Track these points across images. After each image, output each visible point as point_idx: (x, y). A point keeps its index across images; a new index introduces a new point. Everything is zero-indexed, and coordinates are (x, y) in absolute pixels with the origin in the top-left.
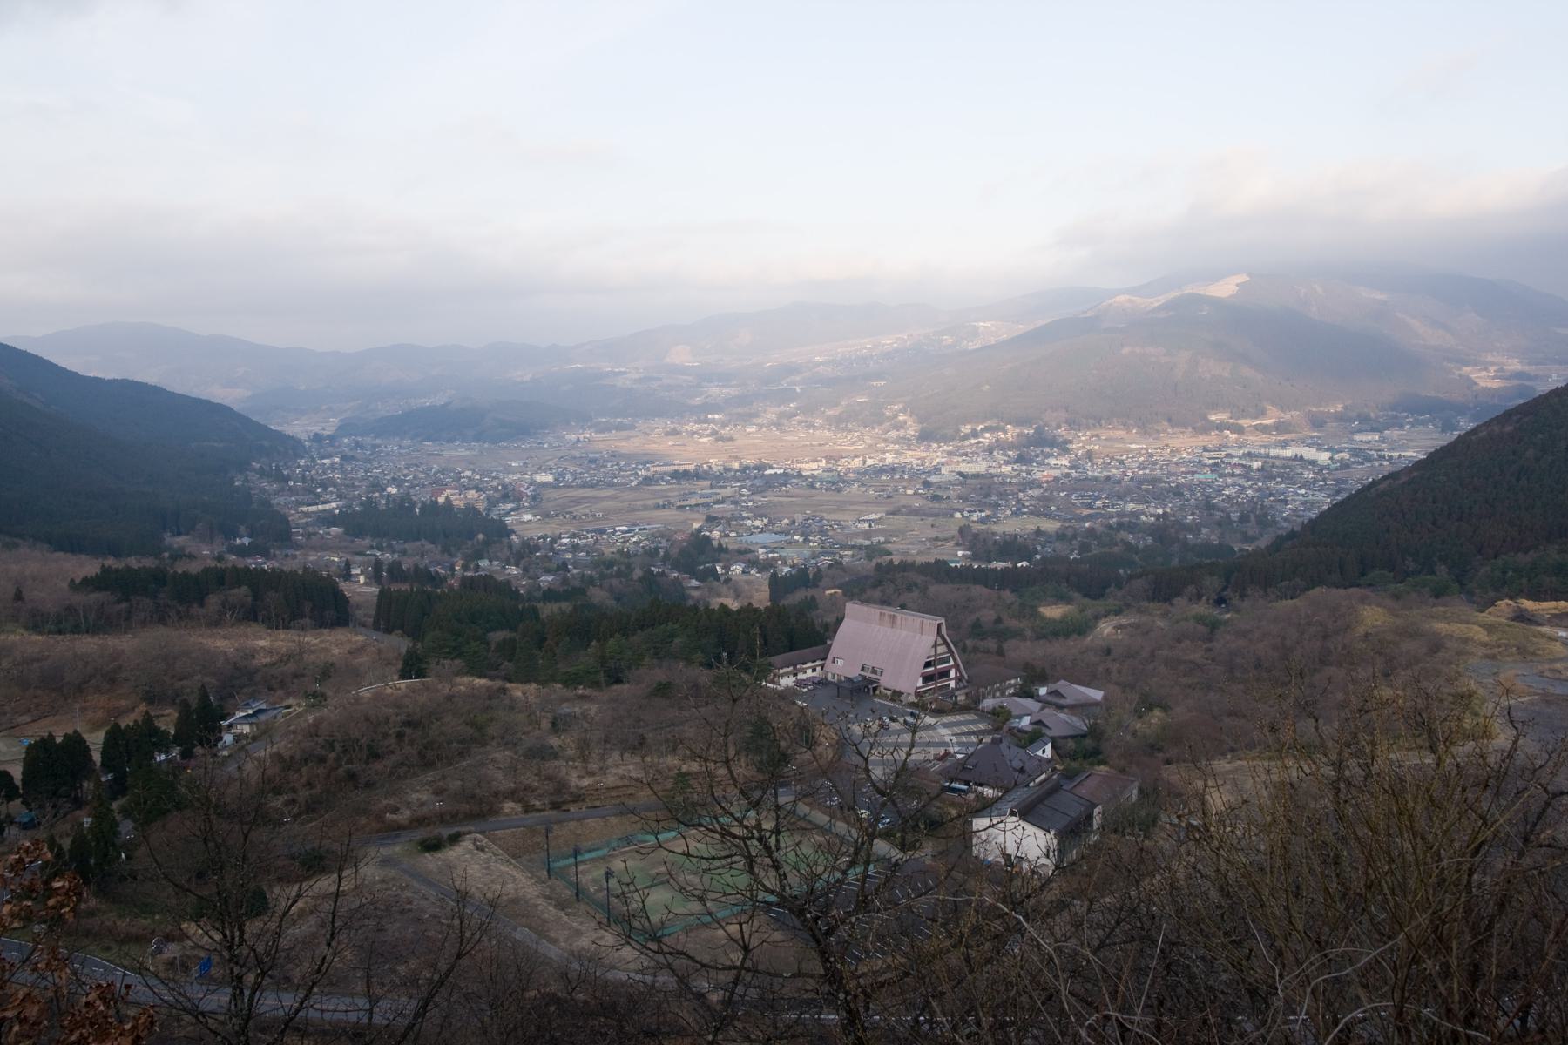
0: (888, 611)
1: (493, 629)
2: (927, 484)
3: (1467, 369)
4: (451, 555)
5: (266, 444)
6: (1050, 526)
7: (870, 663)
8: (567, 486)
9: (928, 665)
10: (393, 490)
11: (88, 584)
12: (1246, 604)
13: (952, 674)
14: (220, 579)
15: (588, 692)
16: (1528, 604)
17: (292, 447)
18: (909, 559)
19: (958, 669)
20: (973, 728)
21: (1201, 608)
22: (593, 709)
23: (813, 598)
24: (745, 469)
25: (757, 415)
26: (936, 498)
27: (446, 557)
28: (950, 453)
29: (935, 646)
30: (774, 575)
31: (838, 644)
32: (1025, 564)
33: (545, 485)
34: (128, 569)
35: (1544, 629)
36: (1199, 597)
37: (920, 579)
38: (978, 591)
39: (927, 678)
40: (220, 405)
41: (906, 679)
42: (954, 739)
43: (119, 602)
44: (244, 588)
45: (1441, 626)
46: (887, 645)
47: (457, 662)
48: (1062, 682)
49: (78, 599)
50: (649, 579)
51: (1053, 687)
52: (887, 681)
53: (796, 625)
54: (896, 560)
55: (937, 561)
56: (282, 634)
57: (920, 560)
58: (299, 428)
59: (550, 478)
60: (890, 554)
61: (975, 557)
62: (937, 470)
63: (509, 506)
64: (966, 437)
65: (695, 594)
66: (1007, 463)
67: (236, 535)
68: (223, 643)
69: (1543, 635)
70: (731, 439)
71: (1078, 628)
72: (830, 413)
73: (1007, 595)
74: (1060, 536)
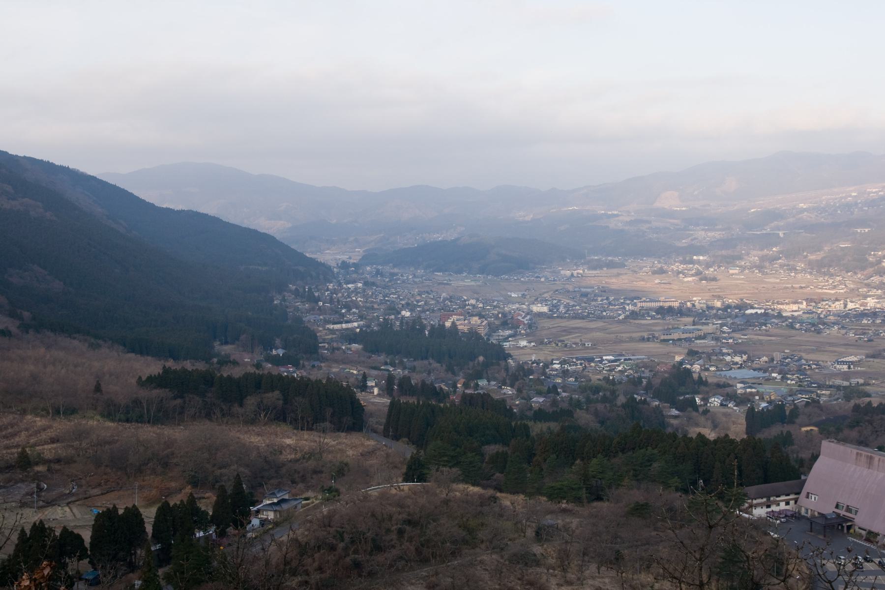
1: (488, 443)
4: (454, 373)
5: (301, 269)
8: (560, 317)
10: (406, 314)
11: (152, 381)
14: (257, 383)
15: (570, 506)
17: (322, 272)
22: (574, 522)
25: (740, 258)
27: (450, 375)
30: (751, 409)
34: (184, 371)
43: (175, 398)
44: (277, 393)
47: (454, 470)
49: (144, 394)
50: (631, 405)
52: (862, 521)
56: (306, 435)
58: (330, 256)
59: (545, 309)
60: (869, 395)
65: (675, 422)
67: (272, 346)
68: (257, 439)
70: (714, 279)
72: (812, 257)
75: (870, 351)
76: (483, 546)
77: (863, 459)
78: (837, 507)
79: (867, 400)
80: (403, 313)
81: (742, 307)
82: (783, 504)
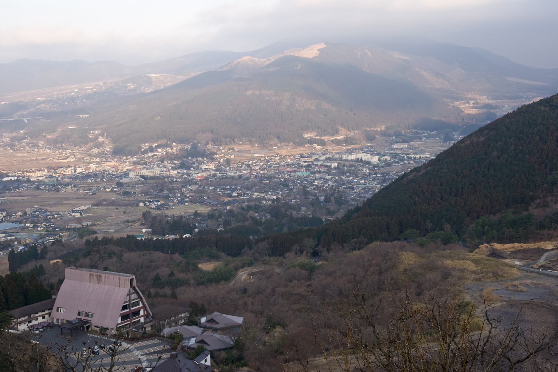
0: (95, 272)
2: (119, 184)
3: (456, 103)
6: (204, 210)
9: (124, 308)
12: (331, 254)
13: (142, 313)
16: (497, 246)
18: (109, 236)
19: (144, 307)
21: (303, 259)
23: (41, 266)
26: (126, 193)
28: (135, 163)
29: (129, 294)
30: (12, 252)
31: (60, 298)
32: (188, 235)
35: (507, 261)
36: (302, 252)
37: (117, 249)
38: (158, 255)
39: (124, 317)
45: (449, 263)
46: (96, 296)
51: (210, 317)
52: (96, 321)
54: (100, 237)
55: (129, 237)
57: (117, 236)
60: (95, 233)
61: (154, 233)
62: (126, 174)
64: (146, 152)
66: (174, 168)
69: (507, 265)
71: (224, 277)
72: (49, 137)
73: (177, 257)
74: (211, 216)
75: (94, 202)
77: (95, 277)
78: (79, 314)
79: (95, 236)
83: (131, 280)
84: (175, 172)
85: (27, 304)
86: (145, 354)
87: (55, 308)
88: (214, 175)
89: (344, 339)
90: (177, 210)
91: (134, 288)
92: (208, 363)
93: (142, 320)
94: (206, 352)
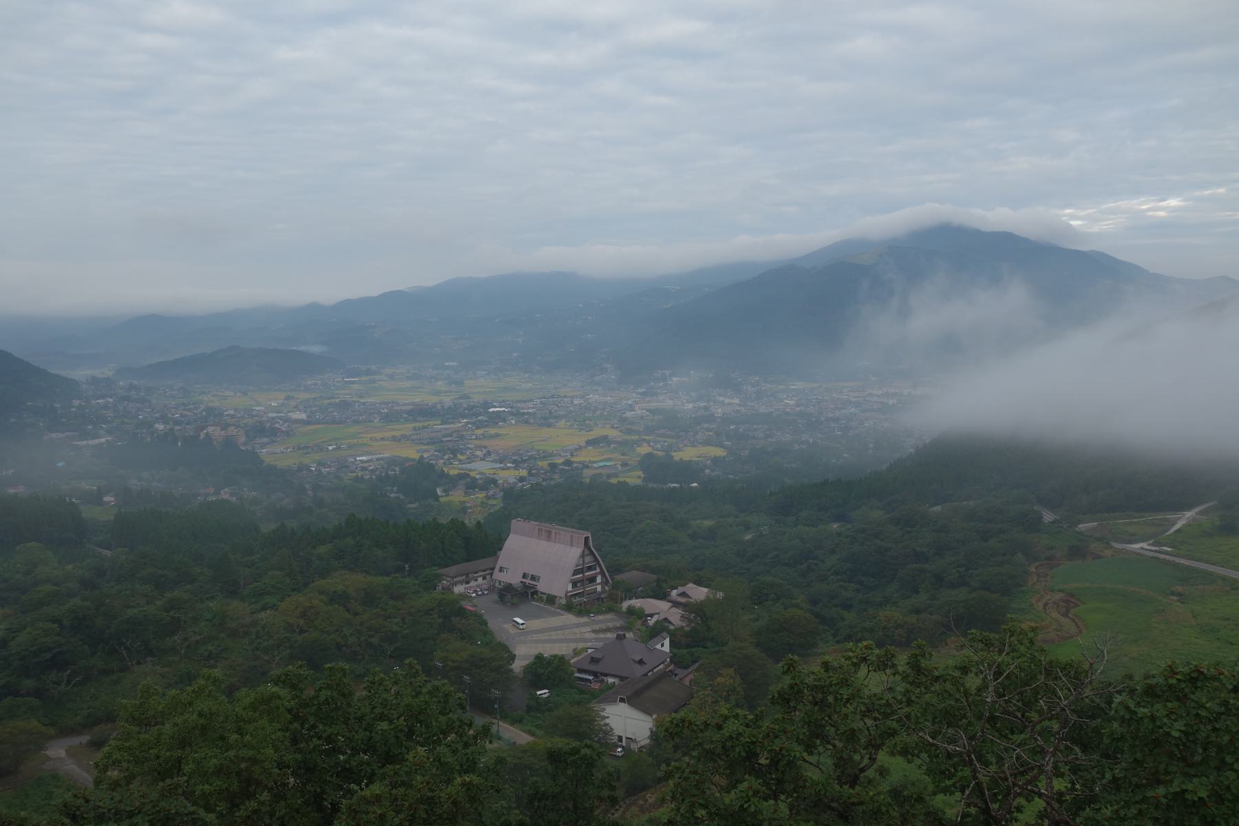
0: (547, 526)
2: (623, 420)
7: (531, 572)
9: (581, 571)
10: (160, 427)
13: (599, 579)
19: (602, 573)
20: (611, 625)
24: (470, 408)
26: (629, 432)
28: (642, 394)
29: (583, 556)
31: (503, 558)
33: (297, 421)
39: (575, 584)
40: (384, 294)
41: (558, 584)
42: (593, 635)
46: (543, 555)
48: (691, 585)
51: (681, 589)
52: (542, 587)
53: (480, 545)
58: (80, 374)
59: (303, 416)
62: (631, 408)
63: (265, 440)
66: (688, 402)
76: (562, 423)
78: (524, 576)
80: (157, 426)
81: (487, 405)
82: (480, 579)
83: (587, 539)
84: (691, 406)
85: (468, 561)
86: (595, 631)
87: (497, 568)
88: (738, 411)
89: (394, 791)
90: (688, 454)
91: (589, 549)
92: (667, 648)
93: (599, 588)
94: (665, 634)
